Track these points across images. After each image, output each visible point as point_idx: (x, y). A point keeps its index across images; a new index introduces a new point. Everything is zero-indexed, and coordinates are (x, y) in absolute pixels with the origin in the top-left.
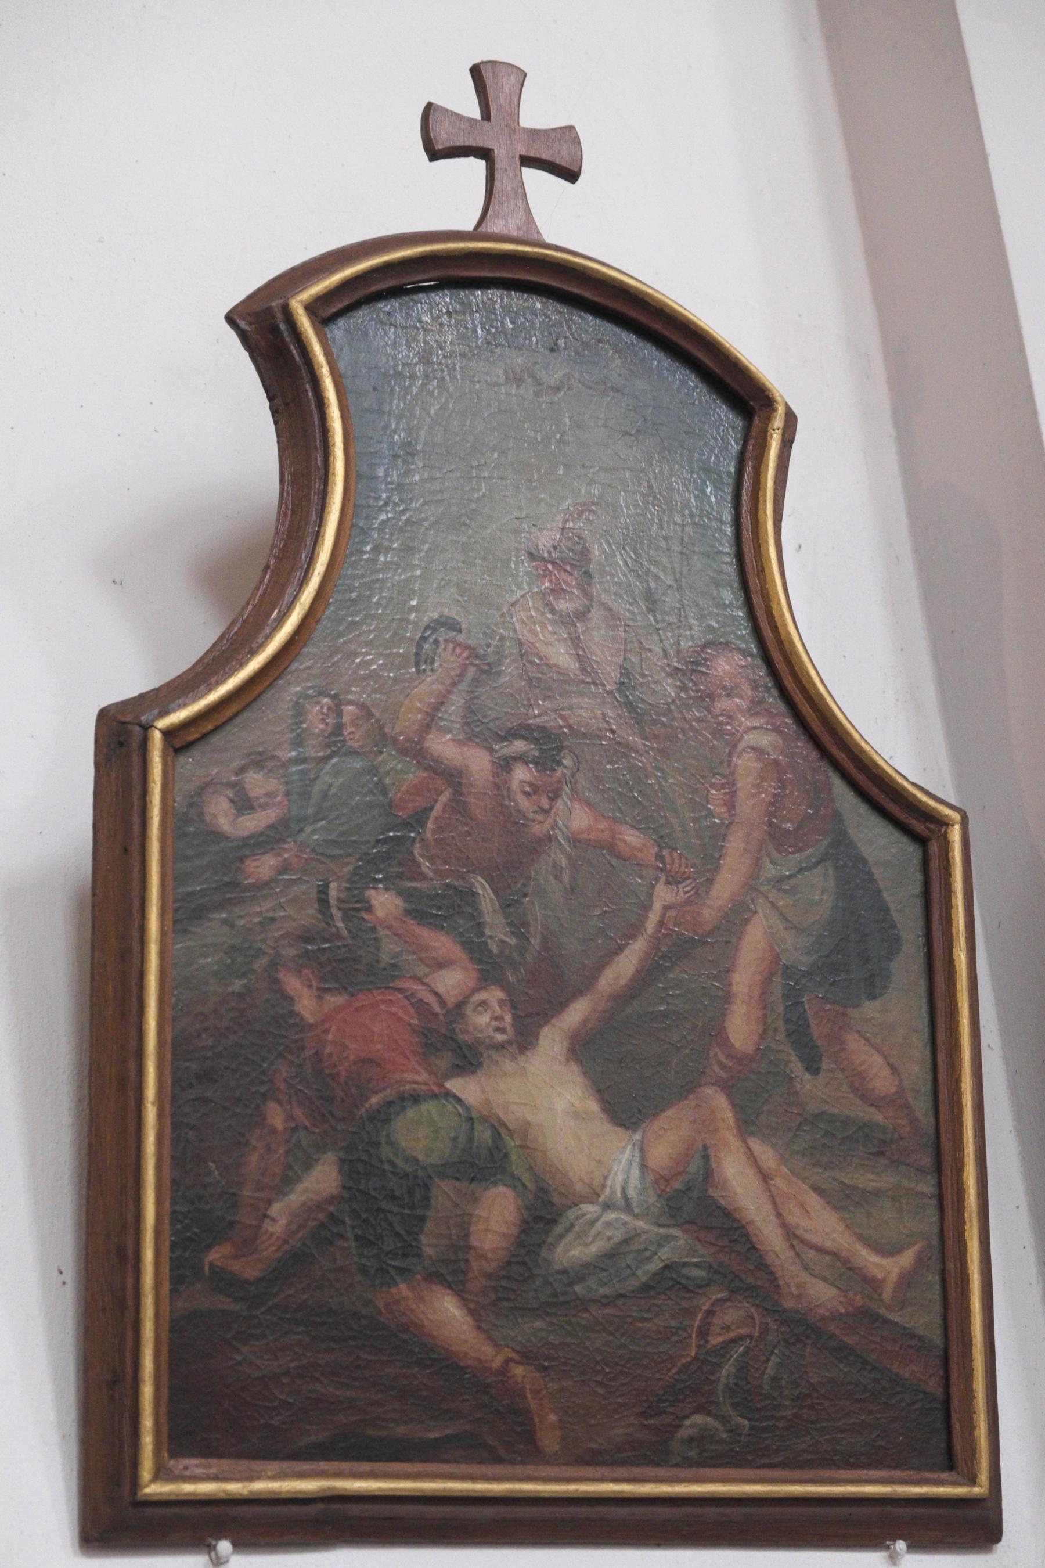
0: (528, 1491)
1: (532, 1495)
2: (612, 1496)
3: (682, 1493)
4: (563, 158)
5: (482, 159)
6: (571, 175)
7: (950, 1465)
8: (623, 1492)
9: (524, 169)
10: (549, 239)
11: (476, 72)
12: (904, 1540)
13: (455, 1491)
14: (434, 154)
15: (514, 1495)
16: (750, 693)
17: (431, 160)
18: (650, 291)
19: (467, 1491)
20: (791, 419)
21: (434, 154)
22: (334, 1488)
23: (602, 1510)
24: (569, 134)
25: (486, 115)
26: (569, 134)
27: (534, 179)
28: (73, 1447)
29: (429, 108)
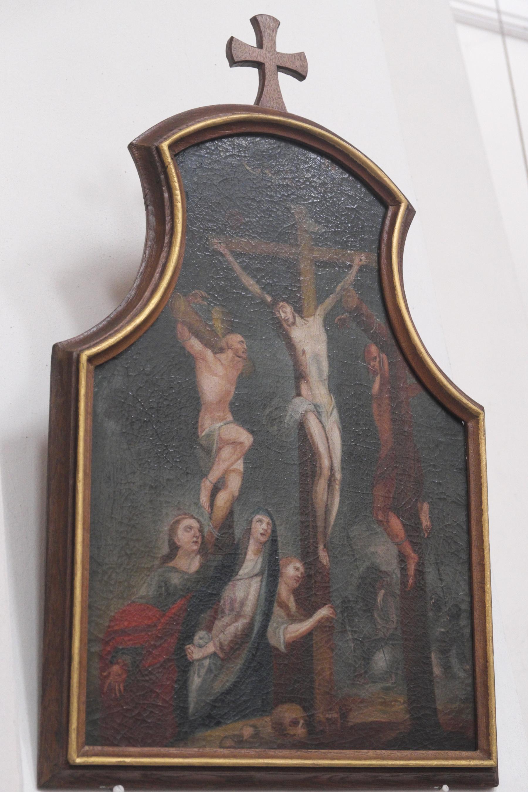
0: (356, 764)
1: (252, 765)
2: (246, 765)
3: (282, 764)
4: (296, 66)
5: (255, 67)
6: (301, 76)
7: (475, 747)
8: (268, 764)
9: (278, 72)
10: (290, 110)
11: (255, 21)
12: (449, 786)
13: (112, 763)
14: (233, 62)
15: (151, 765)
16: (216, 247)
17: (231, 66)
18: (396, 189)
19: (181, 763)
20: (410, 212)
21: (233, 62)
22: (125, 762)
23: (252, 773)
24: (301, 57)
25: (260, 45)
26: (301, 57)
27: (282, 77)
28: (35, 744)
29: (232, 38)
